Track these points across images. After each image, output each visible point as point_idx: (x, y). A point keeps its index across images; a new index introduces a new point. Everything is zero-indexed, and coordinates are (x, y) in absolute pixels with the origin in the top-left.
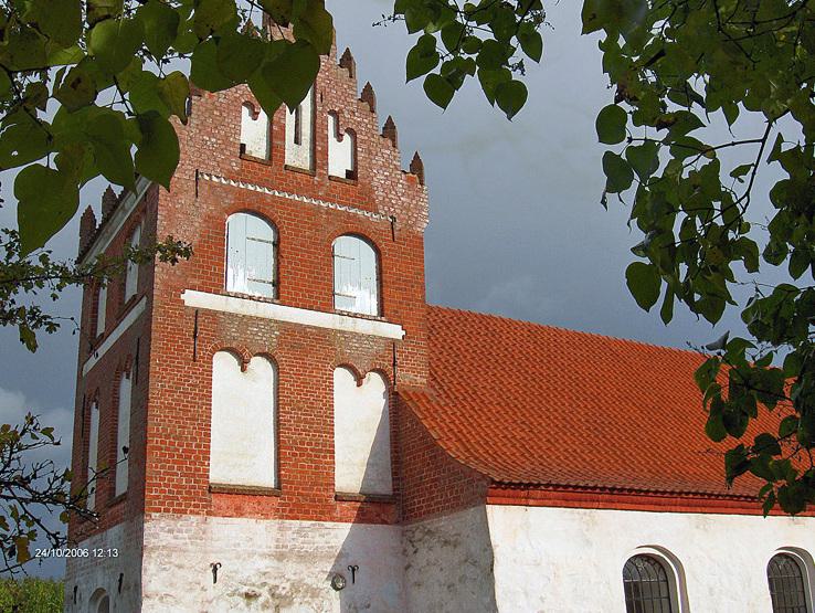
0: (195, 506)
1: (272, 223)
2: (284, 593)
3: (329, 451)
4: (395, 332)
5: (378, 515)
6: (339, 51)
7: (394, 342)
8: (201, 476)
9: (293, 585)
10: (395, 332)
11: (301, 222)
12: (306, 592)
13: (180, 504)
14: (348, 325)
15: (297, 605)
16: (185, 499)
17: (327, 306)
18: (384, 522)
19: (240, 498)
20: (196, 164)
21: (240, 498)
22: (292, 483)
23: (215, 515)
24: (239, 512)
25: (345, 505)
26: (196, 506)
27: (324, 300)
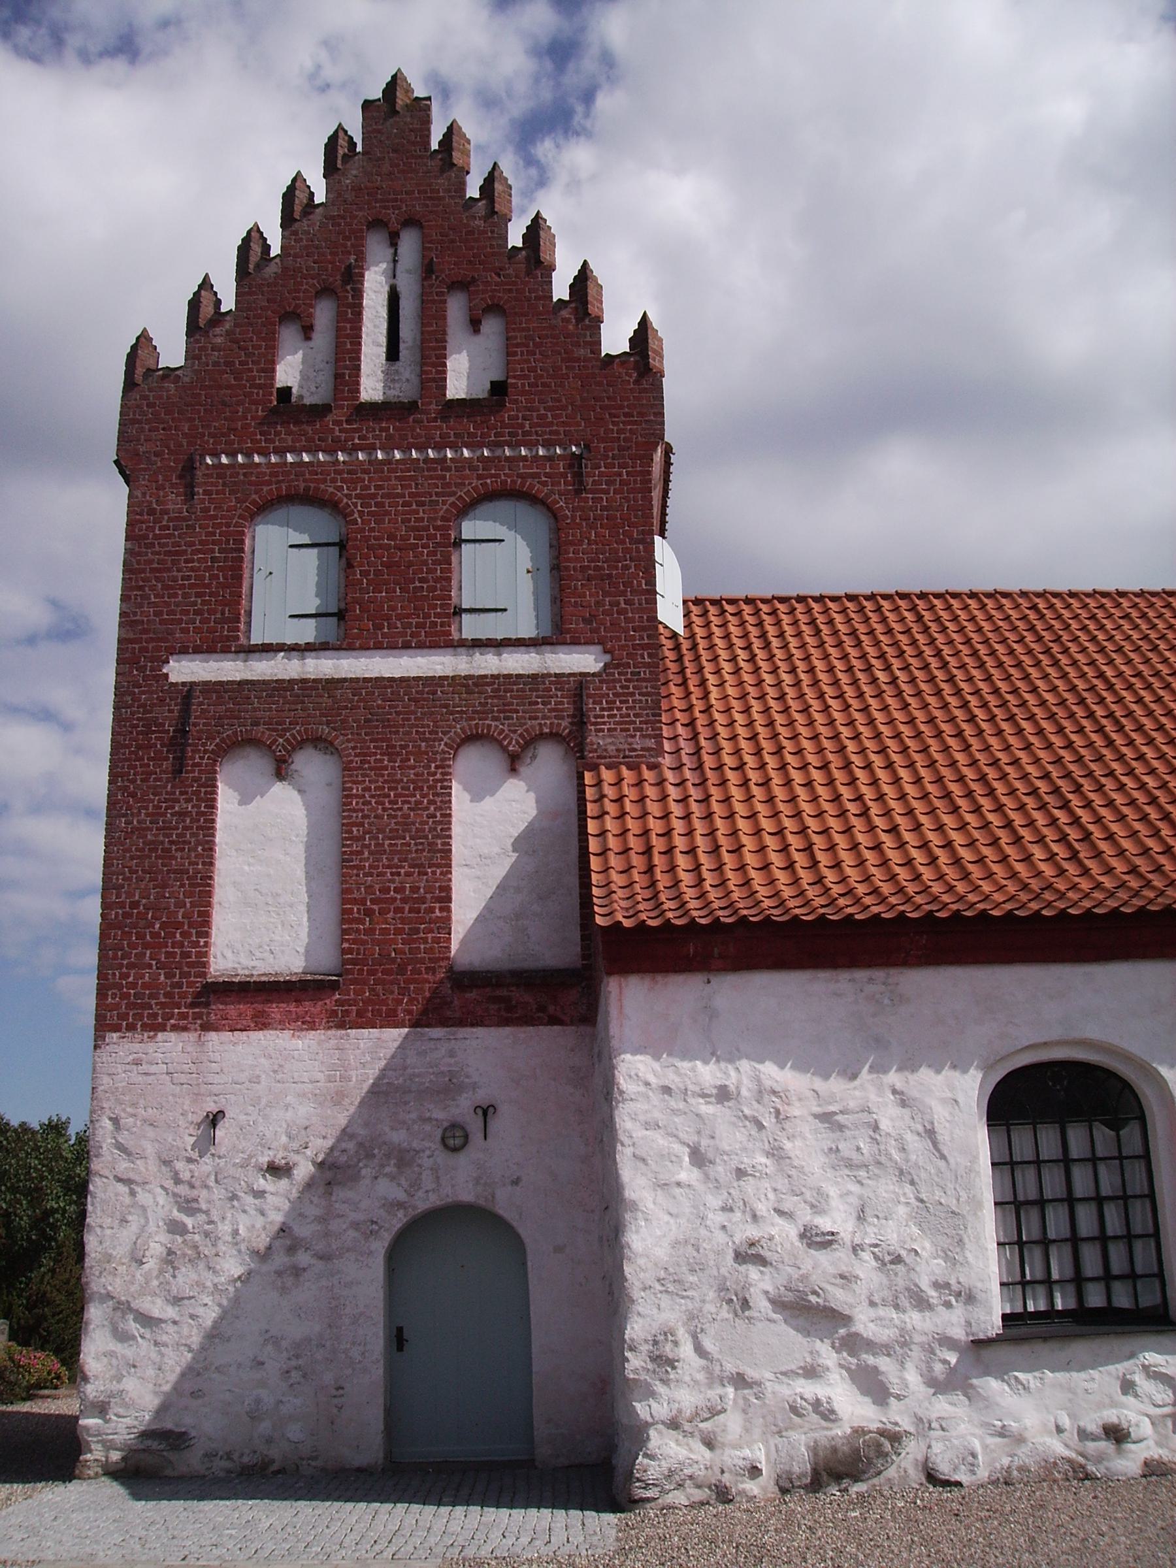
0: (184, 1016)
1: (533, 499)
2: (344, 1158)
3: (439, 900)
4: (584, 661)
5: (542, 1009)
6: (594, 50)
7: (581, 681)
8: (191, 965)
9: (361, 1145)
10: (584, 661)
11: (388, 496)
12: (388, 1156)
13: (155, 1015)
14: (488, 663)
15: (367, 1181)
16: (163, 1005)
17: (439, 639)
18: (554, 1021)
19: (261, 1000)
20: (206, 1165)
21: (261, 1000)
22: (364, 962)
23: (216, 1029)
24: (261, 1023)
25: (472, 995)
26: (184, 1016)
27: (435, 624)
